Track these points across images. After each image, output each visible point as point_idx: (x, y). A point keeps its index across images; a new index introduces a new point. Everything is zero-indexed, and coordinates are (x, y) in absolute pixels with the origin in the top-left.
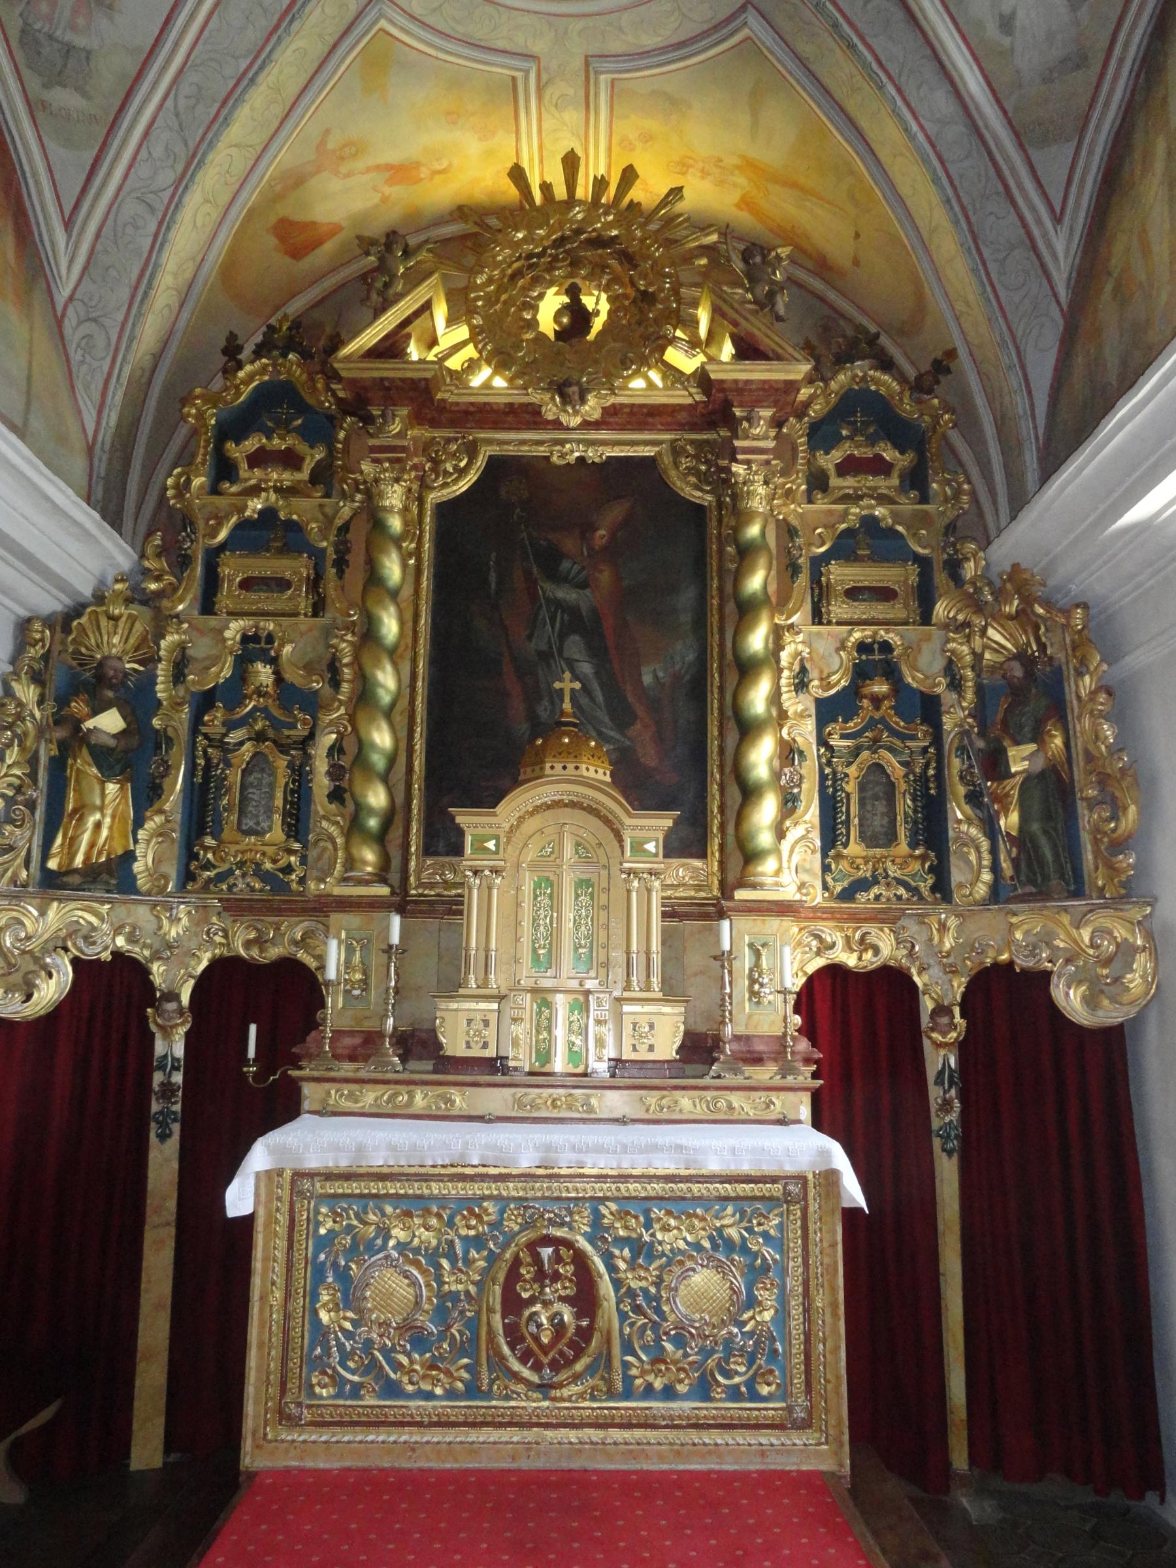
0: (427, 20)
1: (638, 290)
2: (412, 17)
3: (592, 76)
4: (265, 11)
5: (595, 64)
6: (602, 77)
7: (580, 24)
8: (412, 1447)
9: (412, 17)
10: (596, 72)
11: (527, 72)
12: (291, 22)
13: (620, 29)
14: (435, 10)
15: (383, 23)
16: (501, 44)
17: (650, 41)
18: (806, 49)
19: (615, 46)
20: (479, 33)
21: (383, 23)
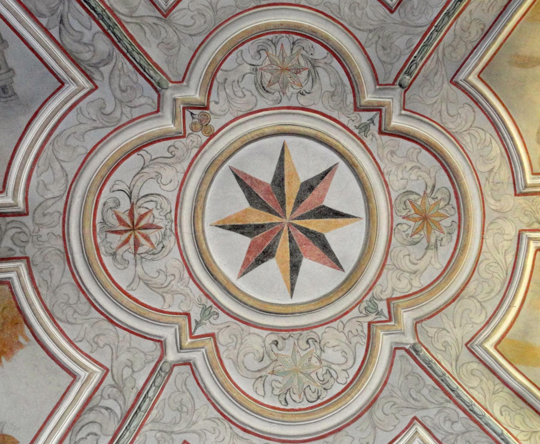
0: (490, 314)
1: (377, 21)
2: (488, 323)
3: (527, 190)
4: (468, 431)
5: (520, 188)
6: (529, 182)
7: (490, 202)
8: (510, 438)
9: (488, 323)
10: (526, 187)
11: (529, 239)
12: (475, 413)
13: (491, 171)
14: (483, 307)
15: (489, 345)
16: (510, 259)
17: (497, 148)
18: (475, 34)
19: (505, 174)
20: (500, 276)
21: (489, 345)
